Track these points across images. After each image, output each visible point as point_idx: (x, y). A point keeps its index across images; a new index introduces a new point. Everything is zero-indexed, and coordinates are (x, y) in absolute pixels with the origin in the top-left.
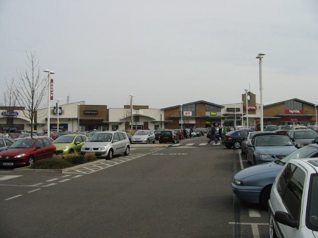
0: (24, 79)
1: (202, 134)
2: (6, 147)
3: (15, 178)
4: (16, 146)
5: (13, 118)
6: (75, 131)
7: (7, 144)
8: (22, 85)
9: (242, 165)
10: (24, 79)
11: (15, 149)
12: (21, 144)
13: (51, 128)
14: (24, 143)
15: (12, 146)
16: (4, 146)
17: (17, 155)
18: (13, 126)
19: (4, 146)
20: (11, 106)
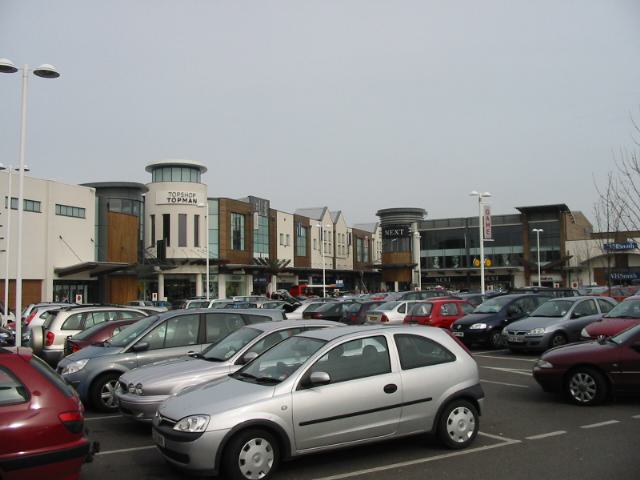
0: (631, 171)
1: (278, 304)
2: (600, 315)
3: (535, 434)
4: (619, 314)
5: (627, 255)
6: (90, 317)
7: (604, 310)
8: (628, 186)
9: (481, 220)
10: (631, 171)
11: (616, 320)
12: (631, 309)
13: (465, 265)
14: (636, 308)
15: (612, 313)
16: (597, 313)
17: (448, 388)
18: (629, 270)
19: (597, 313)
20: (611, 230)
